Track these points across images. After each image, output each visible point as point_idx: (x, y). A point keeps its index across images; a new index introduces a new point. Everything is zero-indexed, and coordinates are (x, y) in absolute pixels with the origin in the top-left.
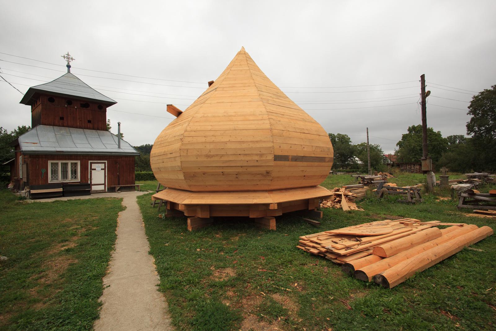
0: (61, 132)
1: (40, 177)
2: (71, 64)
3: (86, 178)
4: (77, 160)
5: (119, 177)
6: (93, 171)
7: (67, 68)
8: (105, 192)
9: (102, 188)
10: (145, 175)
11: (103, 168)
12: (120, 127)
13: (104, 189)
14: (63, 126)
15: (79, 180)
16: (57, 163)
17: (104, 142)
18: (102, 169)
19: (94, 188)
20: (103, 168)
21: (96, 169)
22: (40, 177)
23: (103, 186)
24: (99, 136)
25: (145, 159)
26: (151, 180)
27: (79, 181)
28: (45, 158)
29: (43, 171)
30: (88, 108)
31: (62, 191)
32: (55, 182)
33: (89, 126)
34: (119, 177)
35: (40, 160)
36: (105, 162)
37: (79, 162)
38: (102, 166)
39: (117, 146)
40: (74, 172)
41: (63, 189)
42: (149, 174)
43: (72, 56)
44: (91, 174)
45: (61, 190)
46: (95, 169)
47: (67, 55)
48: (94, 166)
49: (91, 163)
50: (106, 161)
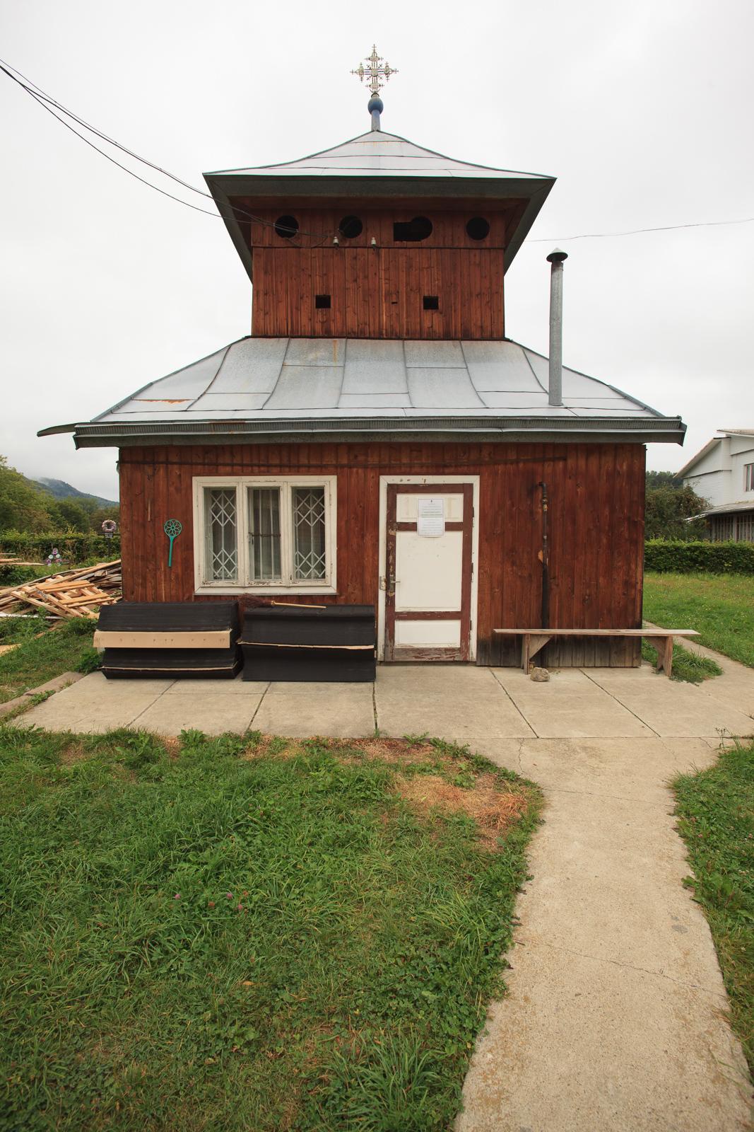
0: (311, 356)
1: (163, 564)
2: (383, 96)
3: (368, 578)
4: (321, 470)
5: (545, 575)
6: (401, 537)
7: (369, 116)
8: (465, 662)
9: (446, 635)
10: (662, 553)
11: (458, 517)
12: (560, 278)
13: (458, 646)
14: (328, 335)
15: (330, 586)
16: (231, 493)
17: (480, 386)
18: (450, 527)
19: (409, 635)
20: (458, 517)
21: (419, 527)
22: (163, 564)
23: (456, 625)
24: (465, 361)
25: (657, 498)
26: (682, 572)
27: (332, 590)
28: (180, 464)
29: (173, 530)
30: (424, 242)
31: (226, 644)
32: (222, 588)
33: (427, 324)
34: (545, 575)
35: (162, 472)
36: (471, 486)
37: (330, 484)
38: (452, 506)
39: (546, 398)
40: (310, 536)
41: (234, 637)
42: (677, 549)
43: (388, 57)
44: (391, 552)
45: (220, 639)
46: (411, 527)
47: (370, 63)
48: (408, 507)
49: (466, 490)
50: (475, 480)
